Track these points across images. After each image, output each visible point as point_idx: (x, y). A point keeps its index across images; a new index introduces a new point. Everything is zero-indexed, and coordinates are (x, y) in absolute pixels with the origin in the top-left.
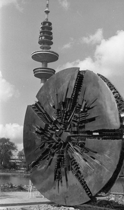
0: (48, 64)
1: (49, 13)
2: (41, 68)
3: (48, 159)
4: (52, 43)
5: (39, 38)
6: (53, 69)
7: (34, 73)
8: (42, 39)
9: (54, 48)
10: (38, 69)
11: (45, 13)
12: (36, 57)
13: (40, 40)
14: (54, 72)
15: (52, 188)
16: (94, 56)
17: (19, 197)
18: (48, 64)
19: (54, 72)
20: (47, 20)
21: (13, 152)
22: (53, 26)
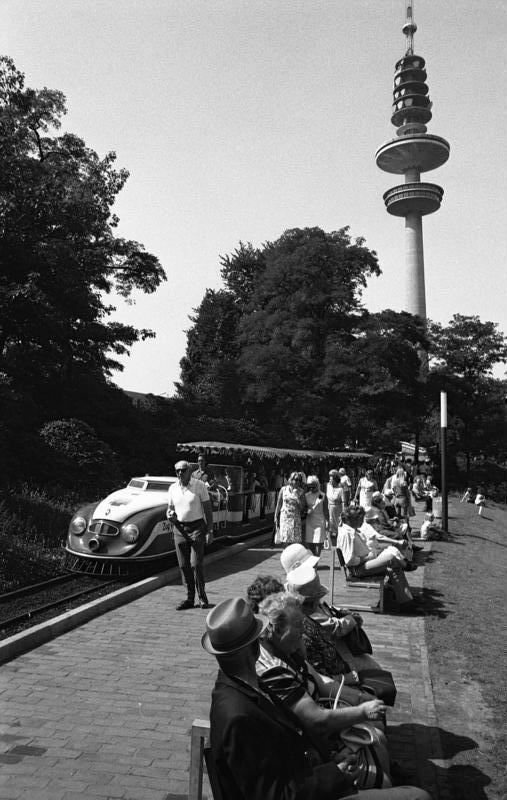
0: (423, 217)
1: (415, 35)
2: (402, 186)
3: (409, 668)
4: (428, 117)
5: (394, 94)
6: (437, 184)
7: (386, 204)
8: (404, 105)
9: (432, 128)
10: (391, 190)
11: (405, 36)
12: (388, 160)
13: (397, 109)
14: (437, 191)
15: (110, 232)
16: (394, 558)
17: (164, 689)
18: (422, 175)
19: (437, 191)
20: (412, 52)
21: (119, 305)
22: (427, 68)
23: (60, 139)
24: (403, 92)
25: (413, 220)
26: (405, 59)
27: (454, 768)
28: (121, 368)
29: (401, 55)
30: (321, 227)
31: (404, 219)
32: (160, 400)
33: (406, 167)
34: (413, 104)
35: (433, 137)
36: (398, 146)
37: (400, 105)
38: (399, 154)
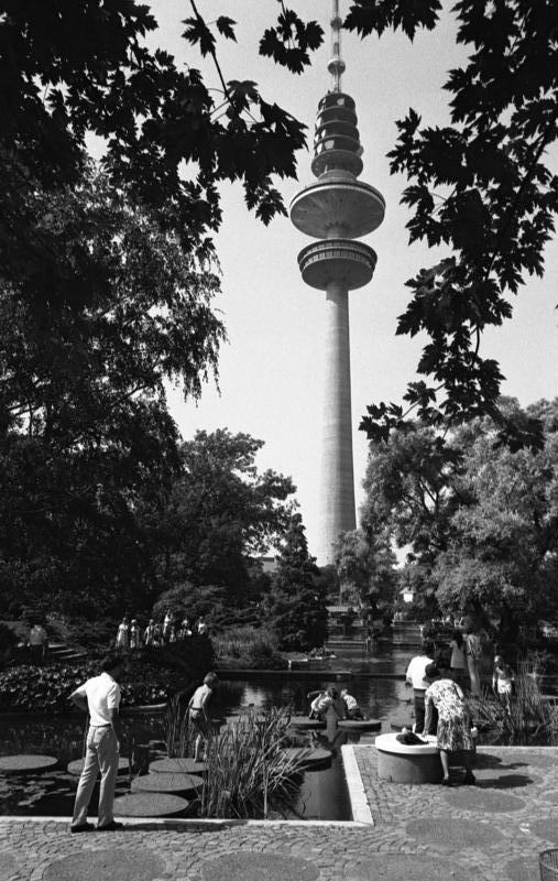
0: (351, 293)
1: (343, 75)
7: (301, 268)
8: (324, 149)
23: (162, 401)
24: (323, 134)
25: (335, 290)
26: (327, 97)
27: (143, 129)
28: (531, 274)
29: (323, 94)
30: (237, 79)
31: (325, 293)
32: (353, 288)
33: (327, 223)
34: (335, 146)
35: (367, 187)
36: (312, 194)
37: (319, 149)
38: (314, 205)
